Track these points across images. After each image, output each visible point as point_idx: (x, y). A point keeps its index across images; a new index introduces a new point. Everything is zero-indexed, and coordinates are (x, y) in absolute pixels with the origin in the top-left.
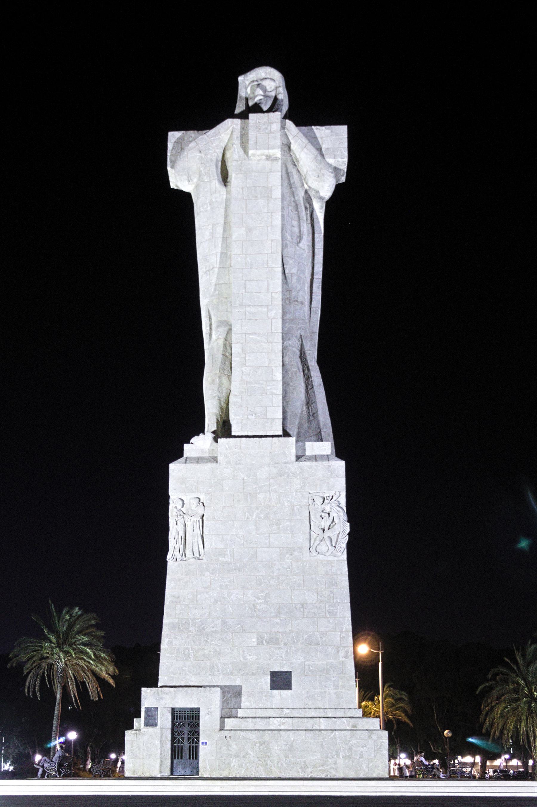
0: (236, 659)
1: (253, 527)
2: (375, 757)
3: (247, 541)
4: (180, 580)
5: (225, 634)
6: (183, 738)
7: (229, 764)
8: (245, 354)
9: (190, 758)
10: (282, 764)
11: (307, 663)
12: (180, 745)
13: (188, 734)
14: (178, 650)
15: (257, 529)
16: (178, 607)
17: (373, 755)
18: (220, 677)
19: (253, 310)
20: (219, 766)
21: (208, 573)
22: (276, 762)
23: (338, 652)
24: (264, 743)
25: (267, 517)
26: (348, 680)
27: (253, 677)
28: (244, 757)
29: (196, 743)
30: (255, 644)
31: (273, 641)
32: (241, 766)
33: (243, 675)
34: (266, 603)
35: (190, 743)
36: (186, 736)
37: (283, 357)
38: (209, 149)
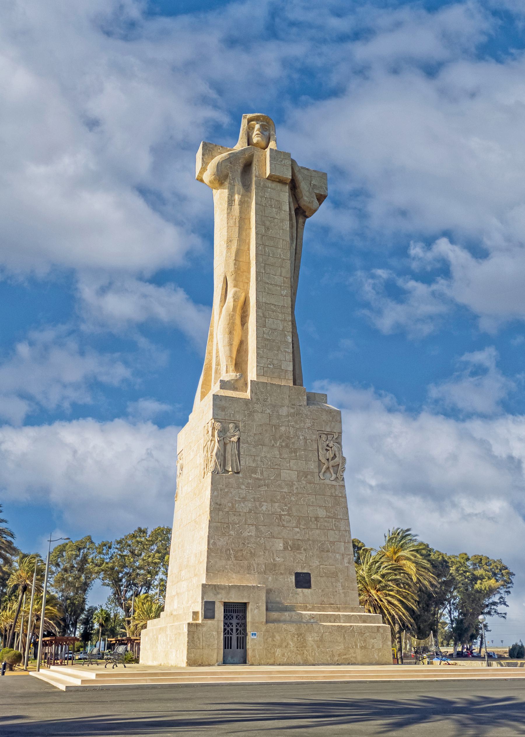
0: (267, 560)
1: (278, 453)
2: (383, 647)
3: (273, 463)
4: (221, 490)
5: (259, 539)
6: (232, 630)
7: (274, 653)
8: (265, 318)
9: (238, 648)
10: (315, 654)
11: (321, 566)
13: (236, 626)
14: (221, 550)
15: (280, 454)
16: (221, 513)
17: (381, 646)
18: (256, 576)
19: (271, 286)
20: (266, 655)
21: (243, 487)
22: (310, 652)
23: (343, 558)
24: (301, 634)
25: (287, 446)
26: (351, 582)
27: (281, 576)
28: (286, 647)
29: (231, 634)
30: (282, 548)
31: (296, 548)
32: (283, 655)
33: (274, 575)
34: (289, 515)
35: (238, 634)
38: (237, 163)
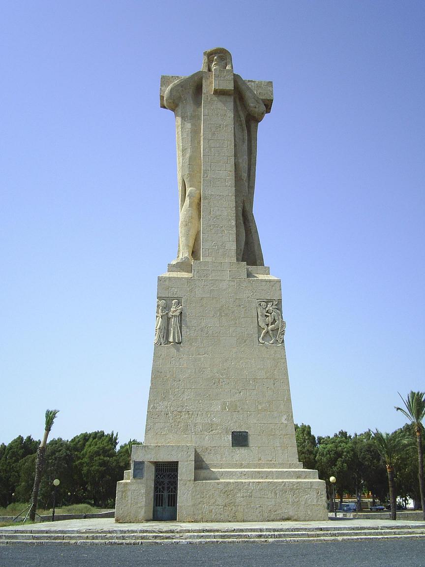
12: (161, 493)
13: (168, 484)
36: (166, 486)
37: (235, 156)
